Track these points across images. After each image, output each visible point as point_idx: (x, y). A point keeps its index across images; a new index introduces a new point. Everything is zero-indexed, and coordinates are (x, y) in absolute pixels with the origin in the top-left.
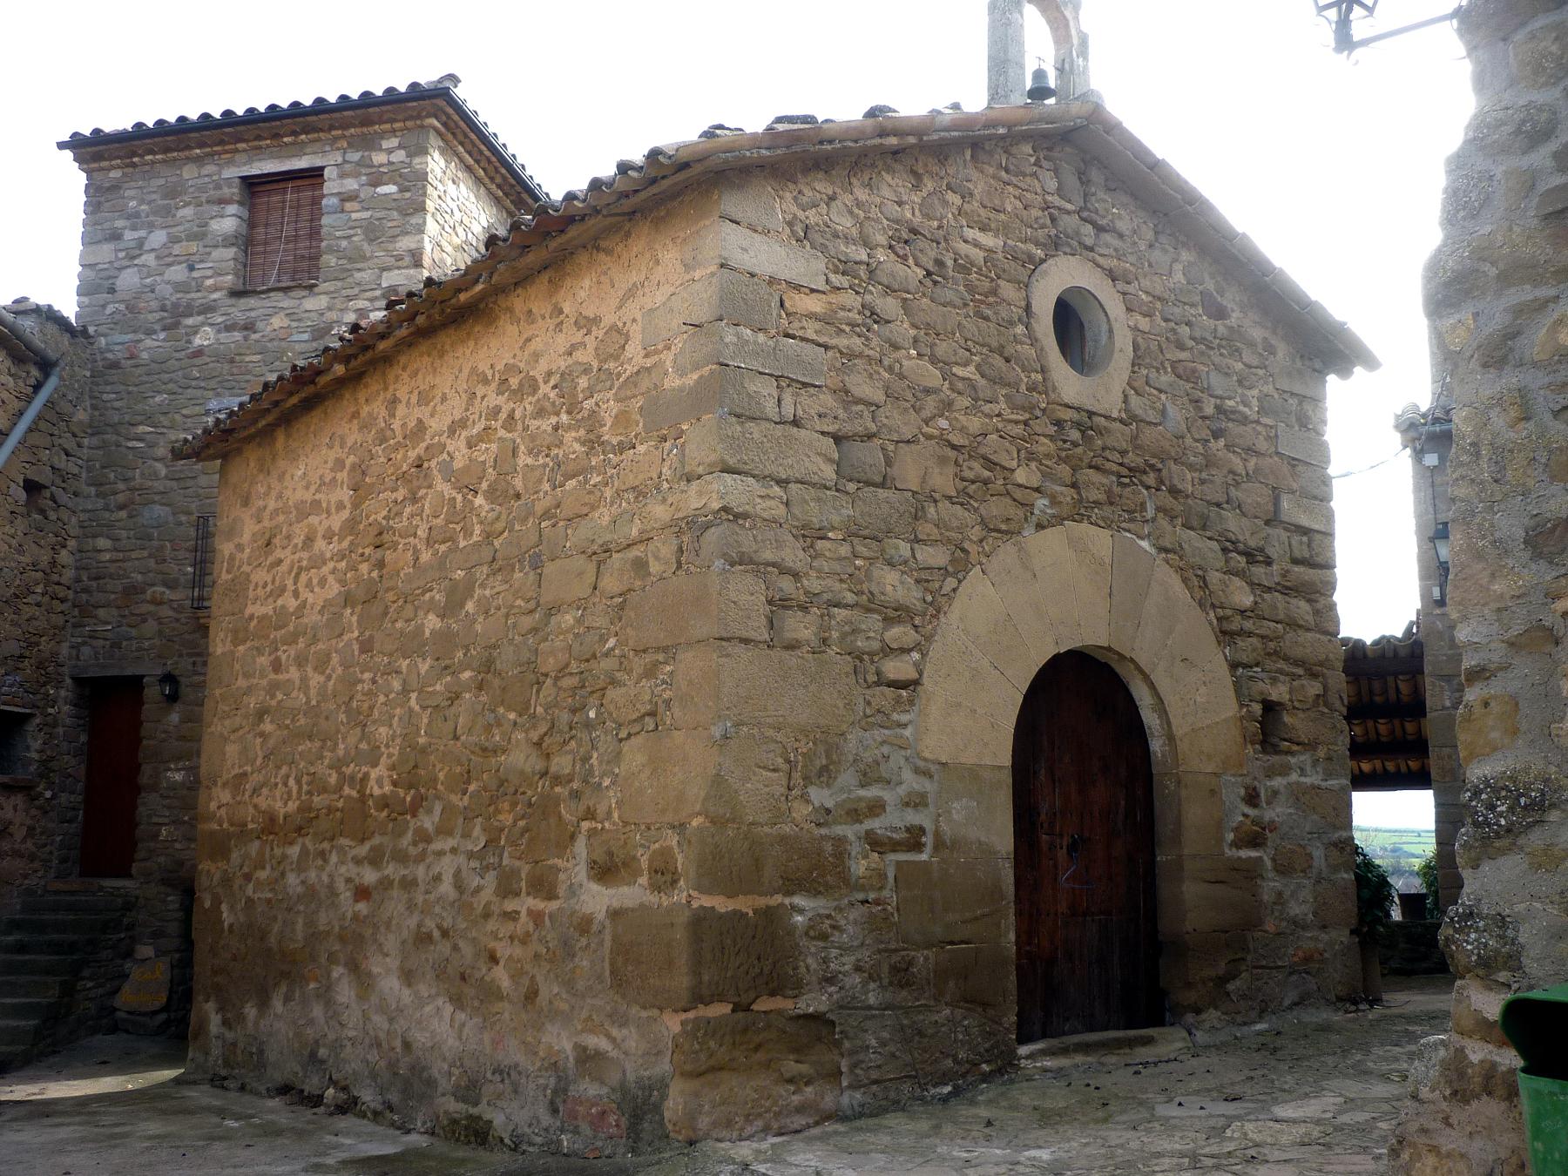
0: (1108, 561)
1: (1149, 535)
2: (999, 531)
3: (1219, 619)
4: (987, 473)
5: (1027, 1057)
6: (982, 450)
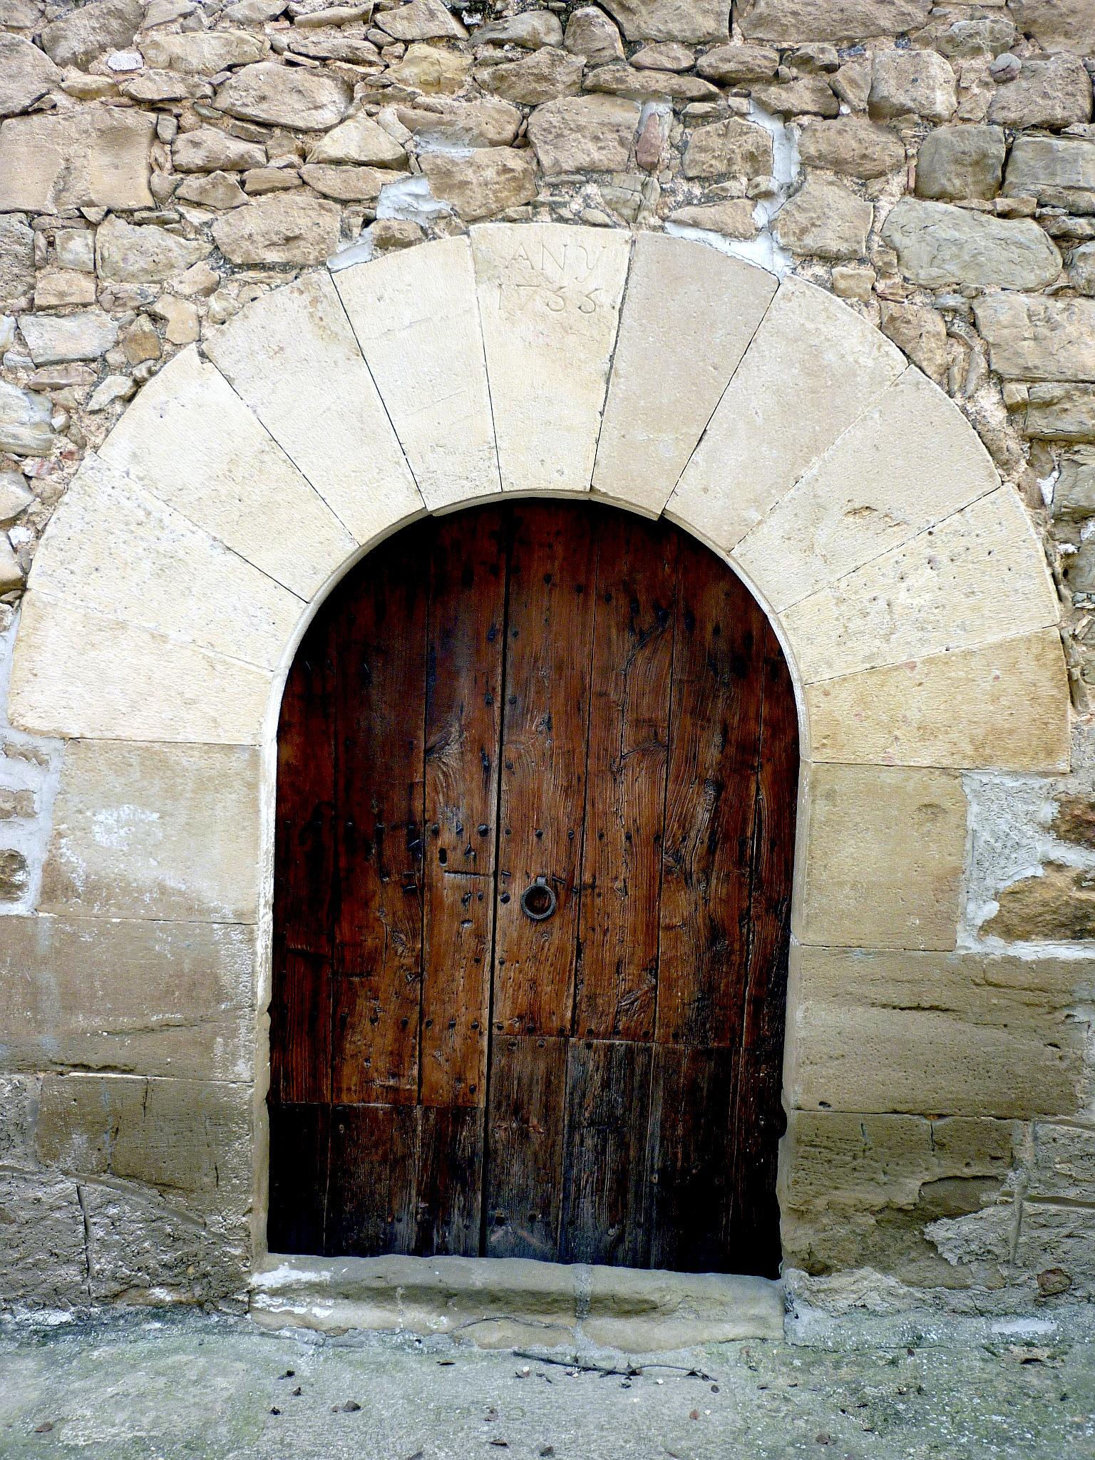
0: (608, 298)
1: (771, 226)
2: (262, 266)
3: (1013, 409)
4: (237, 148)
5: (274, 1293)
6: (223, 101)
